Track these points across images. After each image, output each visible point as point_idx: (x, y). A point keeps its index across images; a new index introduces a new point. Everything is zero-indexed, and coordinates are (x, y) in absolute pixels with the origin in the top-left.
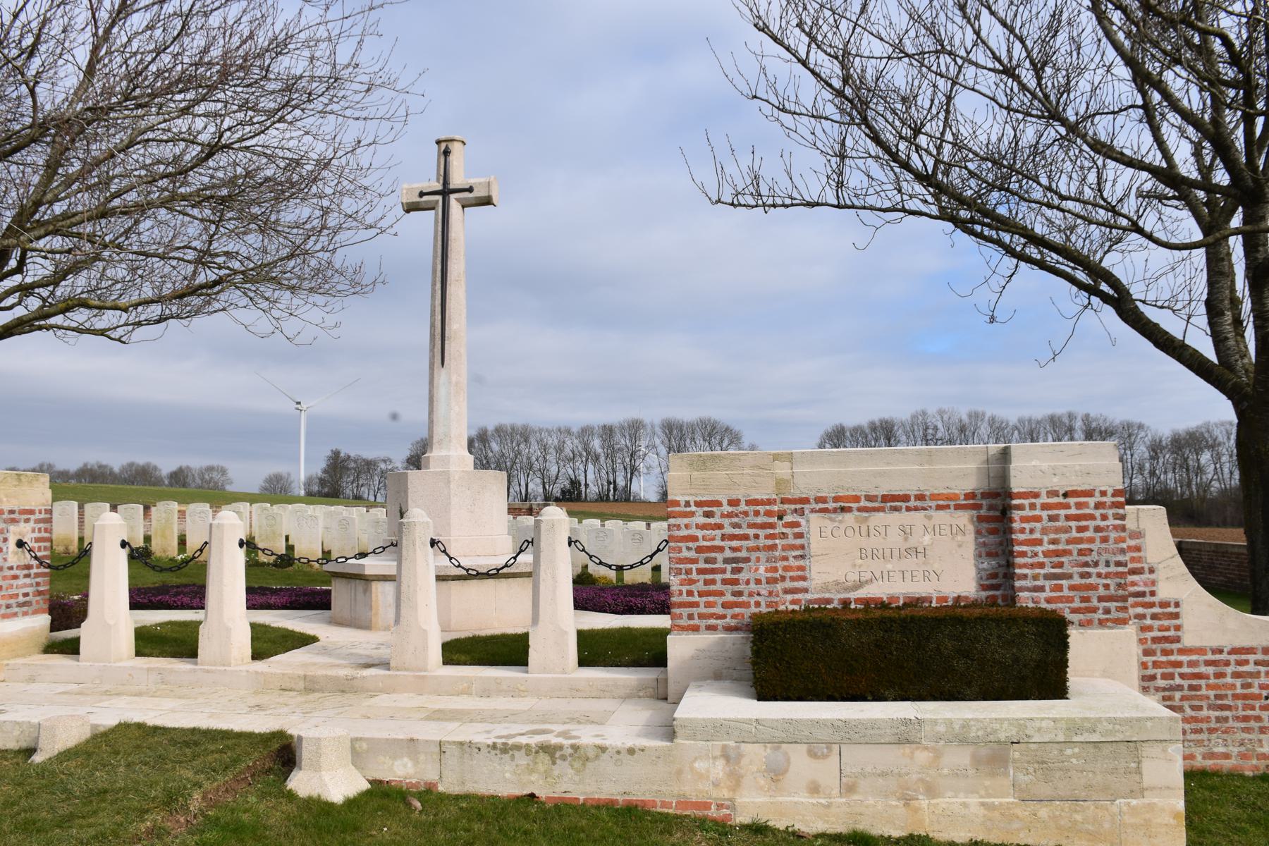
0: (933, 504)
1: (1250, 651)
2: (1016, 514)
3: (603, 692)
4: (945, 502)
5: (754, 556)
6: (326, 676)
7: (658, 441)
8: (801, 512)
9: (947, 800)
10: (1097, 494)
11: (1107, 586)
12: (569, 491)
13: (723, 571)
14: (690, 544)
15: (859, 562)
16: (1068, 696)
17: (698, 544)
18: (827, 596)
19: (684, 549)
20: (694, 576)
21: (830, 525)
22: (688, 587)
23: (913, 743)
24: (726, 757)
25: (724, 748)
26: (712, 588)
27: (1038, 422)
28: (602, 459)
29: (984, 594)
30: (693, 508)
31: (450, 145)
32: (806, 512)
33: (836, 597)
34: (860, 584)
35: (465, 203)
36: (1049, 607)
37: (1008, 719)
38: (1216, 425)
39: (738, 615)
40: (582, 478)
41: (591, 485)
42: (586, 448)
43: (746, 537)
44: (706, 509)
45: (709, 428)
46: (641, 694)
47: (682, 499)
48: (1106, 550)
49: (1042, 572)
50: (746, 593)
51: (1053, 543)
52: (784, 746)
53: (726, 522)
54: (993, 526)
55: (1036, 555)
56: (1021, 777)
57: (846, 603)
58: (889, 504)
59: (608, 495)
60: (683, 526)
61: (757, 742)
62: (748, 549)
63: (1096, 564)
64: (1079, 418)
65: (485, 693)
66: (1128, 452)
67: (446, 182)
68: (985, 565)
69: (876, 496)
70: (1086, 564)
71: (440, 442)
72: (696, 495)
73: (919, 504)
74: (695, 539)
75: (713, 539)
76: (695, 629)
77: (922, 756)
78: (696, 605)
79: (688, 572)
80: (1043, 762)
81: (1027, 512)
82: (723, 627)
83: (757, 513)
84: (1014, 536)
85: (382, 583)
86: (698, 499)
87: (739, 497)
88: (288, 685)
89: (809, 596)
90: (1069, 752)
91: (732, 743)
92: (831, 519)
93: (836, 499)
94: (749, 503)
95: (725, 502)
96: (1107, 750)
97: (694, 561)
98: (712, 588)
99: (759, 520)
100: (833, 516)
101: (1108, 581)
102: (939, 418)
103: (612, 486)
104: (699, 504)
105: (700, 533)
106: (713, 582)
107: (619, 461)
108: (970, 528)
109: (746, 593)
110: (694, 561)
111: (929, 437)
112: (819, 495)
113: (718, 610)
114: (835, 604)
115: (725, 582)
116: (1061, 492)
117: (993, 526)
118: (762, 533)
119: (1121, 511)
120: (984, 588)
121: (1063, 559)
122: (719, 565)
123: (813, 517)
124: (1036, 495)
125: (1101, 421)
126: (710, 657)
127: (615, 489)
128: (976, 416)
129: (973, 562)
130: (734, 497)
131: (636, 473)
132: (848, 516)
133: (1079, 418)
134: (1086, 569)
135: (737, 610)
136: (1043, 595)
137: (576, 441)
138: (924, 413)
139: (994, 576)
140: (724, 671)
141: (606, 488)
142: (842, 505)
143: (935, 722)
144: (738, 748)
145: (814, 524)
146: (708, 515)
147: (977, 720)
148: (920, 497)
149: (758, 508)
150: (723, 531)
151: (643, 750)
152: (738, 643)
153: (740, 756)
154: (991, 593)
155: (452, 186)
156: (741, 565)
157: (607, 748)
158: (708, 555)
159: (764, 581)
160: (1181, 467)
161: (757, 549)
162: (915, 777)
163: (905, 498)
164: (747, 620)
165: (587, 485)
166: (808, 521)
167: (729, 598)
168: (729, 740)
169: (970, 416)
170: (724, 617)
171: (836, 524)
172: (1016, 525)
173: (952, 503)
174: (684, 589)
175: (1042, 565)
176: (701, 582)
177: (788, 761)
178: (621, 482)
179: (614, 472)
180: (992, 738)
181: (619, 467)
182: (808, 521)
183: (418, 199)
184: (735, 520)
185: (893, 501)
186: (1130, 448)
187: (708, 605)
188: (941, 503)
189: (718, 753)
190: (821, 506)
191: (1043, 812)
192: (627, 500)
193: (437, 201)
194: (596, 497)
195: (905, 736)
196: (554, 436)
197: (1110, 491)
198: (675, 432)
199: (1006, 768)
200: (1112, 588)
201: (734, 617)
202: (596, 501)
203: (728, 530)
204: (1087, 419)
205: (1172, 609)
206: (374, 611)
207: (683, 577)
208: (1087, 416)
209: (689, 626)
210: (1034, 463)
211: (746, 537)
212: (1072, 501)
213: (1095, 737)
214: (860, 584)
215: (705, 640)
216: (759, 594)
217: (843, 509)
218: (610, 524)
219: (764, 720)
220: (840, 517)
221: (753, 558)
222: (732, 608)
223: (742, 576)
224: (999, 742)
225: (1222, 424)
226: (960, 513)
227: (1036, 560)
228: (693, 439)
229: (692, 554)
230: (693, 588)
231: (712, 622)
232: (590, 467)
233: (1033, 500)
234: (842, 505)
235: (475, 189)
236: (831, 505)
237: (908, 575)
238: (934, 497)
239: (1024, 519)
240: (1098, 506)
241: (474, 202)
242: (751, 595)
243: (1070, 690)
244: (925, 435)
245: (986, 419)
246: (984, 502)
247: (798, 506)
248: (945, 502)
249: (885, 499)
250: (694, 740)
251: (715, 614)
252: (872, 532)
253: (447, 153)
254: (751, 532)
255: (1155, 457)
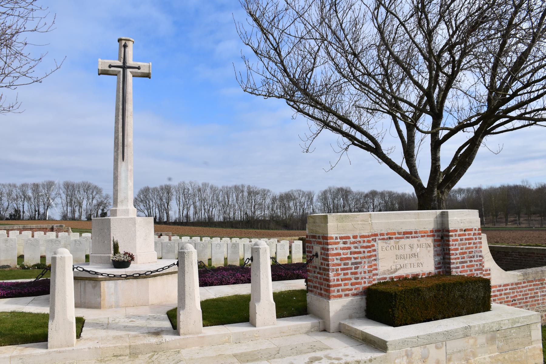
0: (420, 235)
1: (508, 285)
2: (451, 239)
3: (295, 332)
4: (424, 234)
5: (363, 260)
6: (144, 344)
7: (61, 192)
8: (375, 240)
9: (479, 358)
10: (474, 230)
11: (477, 265)
12: (14, 215)
13: (351, 269)
14: (338, 257)
15: (396, 260)
16: (491, 309)
17: (340, 257)
18: (385, 276)
19: (335, 259)
20: (340, 272)
21: (385, 245)
22: (337, 277)
23: (469, 336)
24: (407, 355)
25: (406, 351)
26: (347, 277)
27: (230, 188)
28: (32, 200)
29: (437, 271)
30: (339, 240)
31: (127, 42)
32: (377, 240)
33: (388, 276)
34: (396, 270)
35: (135, 74)
36: (462, 274)
37: (495, 322)
38: (295, 191)
39: (357, 288)
40: (21, 209)
41: (26, 212)
42: (24, 193)
43: (360, 253)
44: (344, 240)
45: (87, 186)
46: (312, 330)
47: (334, 236)
48: (476, 251)
49: (459, 261)
50: (360, 278)
51: (345, 244)
52: (427, 346)
53: (352, 246)
54: (438, 243)
55: (457, 254)
56: (501, 344)
57: (392, 279)
58: (405, 236)
59: (35, 217)
60: (335, 249)
61: (418, 346)
62: (361, 258)
63: (474, 257)
64: (246, 187)
65: (238, 342)
66: (264, 201)
67: (124, 62)
68: (437, 259)
69: (401, 232)
70: (471, 257)
71: (122, 202)
72: (340, 234)
73: (415, 235)
74: (339, 254)
75: (347, 254)
76: (340, 296)
77: (471, 341)
78: (340, 285)
79: (337, 270)
80: (506, 337)
81: (454, 238)
82: (352, 294)
83: (364, 241)
84: (450, 247)
85: (107, 282)
86: (340, 236)
87: (357, 234)
88: (119, 353)
89: (378, 277)
90: (512, 331)
91: (409, 349)
92: (386, 243)
93: (387, 234)
94: (361, 237)
95: (351, 237)
96: (522, 328)
97: (339, 265)
98: (347, 277)
99: (365, 244)
100: (386, 241)
101: (477, 263)
102: (190, 185)
103: (37, 213)
104: (341, 238)
105: (341, 252)
106: (347, 274)
107: (42, 201)
108: (432, 245)
109: (360, 278)
110: (339, 265)
111: (185, 193)
112: (382, 232)
113: (349, 287)
114: (388, 279)
115: (352, 273)
116: (464, 229)
117: (438, 243)
118: (366, 250)
119: (480, 236)
120: (436, 268)
121: (465, 255)
122: (349, 266)
123: (380, 241)
124: (456, 231)
125: (254, 189)
126: (347, 309)
127: (39, 214)
128: (205, 185)
129: (433, 258)
130: (355, 234)
131: (50, 206)
132: (392, 241)
133: (246, 187)
134: (471, 259)
135: (357, 286)
136: (459, 270)
137: (19, 191)
138: (184, 183)
139: (439, 263)
140: (353, 314)
141: (34, 213)
142: (389, 237)
143: (475, 326)
144: (411, 350)
145: (380, 245)
146: (345, 243)
147: (487, 324)
148: (416, 232)
149: (365, 239)
150: (351, 250)
151: (375, 359)
152: (360, 302)
153: (412, 353)
154: (439, 270)
155: (128, 65)
156: (358, 265)
157: (360, 361)
158: (345, 261)
159: (367, 272)
160: (283, 207)
161: (364, 258)
162: (469, 350)
163: (411, 233)
164: (361, 290)
165: (24, 212)
166: (377, 244)
167: (353, 281)
168: (408, 347)
169: (203, 185)
170: (351, 290)
171: (388, 245)
172: (451, 243)
173: (426, 234)
174: (336, 278)
175: (458, 258)
176: (342, 274)
177: (429, 352)
178: (42, 211)
179: (38, 206)
180: (491, 330)
181: (41, 203)
182: (377, 244)
183: (108, 69)
184: (356, 245)
185: (407, 234)
186: (264, 199)
187: (345, 285)
188: (423, 234)
189: (404, 354)
190: (382, 237)
191: (507, 357)
192: (45, 219)
193: (120, 72)
194: (28, 218)
195: (466, 333)
196: (7, 188)
197: (477, 229)
198: (70, 187)
199: (495, 341)
200: (478, 265)
201: (355, 289)
202: (29, 220)
203: (353, 250)
204: (249, 188)
205: (488, 272)
206: (102, 298)
207: (335, 272)
208: (249, 186)
209: (338, 295)
210: (455, 218)
211: (360, 253)
212: (467, 233)
213: (519, 325)
214: (396, 270)
215: (345, 301)
216: (365, 278)
217: (390, 238)
218: (37, 234)
219: (420, 336)
220: (389, 241)
221: (363, 262)
222: (355, 285)
223: (359, 270)
224: (493, 331)
225: (297, 191)
226: (428, 238)
227: (457, 256)
228: (79, 191)
229: (339, 262)
230: (339, 277)
231: (347, 292)
232: (26, 204)
233: (456, 233)
234: (389, 237)
235: (142, 68)
236: (386, 237)
237: (412, 265)
238: (421, 232)
239: (454, 241)
240: (474, 234)
241: (140, 75)
242: (362, 279)
243: (492, 307)
244: (184, 192)
245: (209, 186)
246: (436, 234)
247: (374, 237)
248: (424, 234)
249: (405, 233)
250: (395, 350)
251: (348, 289)
252: (400, 247)
253: (125, 46)
254: (362, 250)
255: (273, 203)
